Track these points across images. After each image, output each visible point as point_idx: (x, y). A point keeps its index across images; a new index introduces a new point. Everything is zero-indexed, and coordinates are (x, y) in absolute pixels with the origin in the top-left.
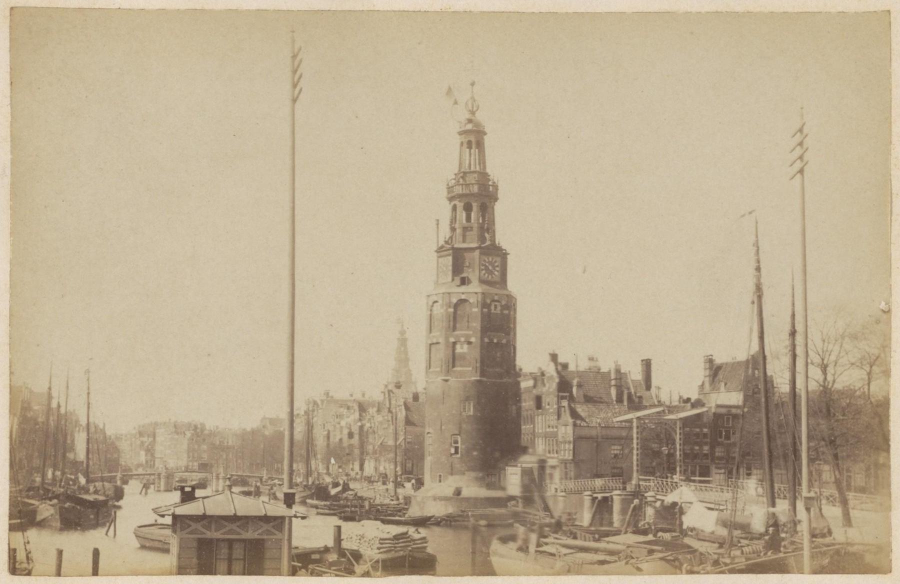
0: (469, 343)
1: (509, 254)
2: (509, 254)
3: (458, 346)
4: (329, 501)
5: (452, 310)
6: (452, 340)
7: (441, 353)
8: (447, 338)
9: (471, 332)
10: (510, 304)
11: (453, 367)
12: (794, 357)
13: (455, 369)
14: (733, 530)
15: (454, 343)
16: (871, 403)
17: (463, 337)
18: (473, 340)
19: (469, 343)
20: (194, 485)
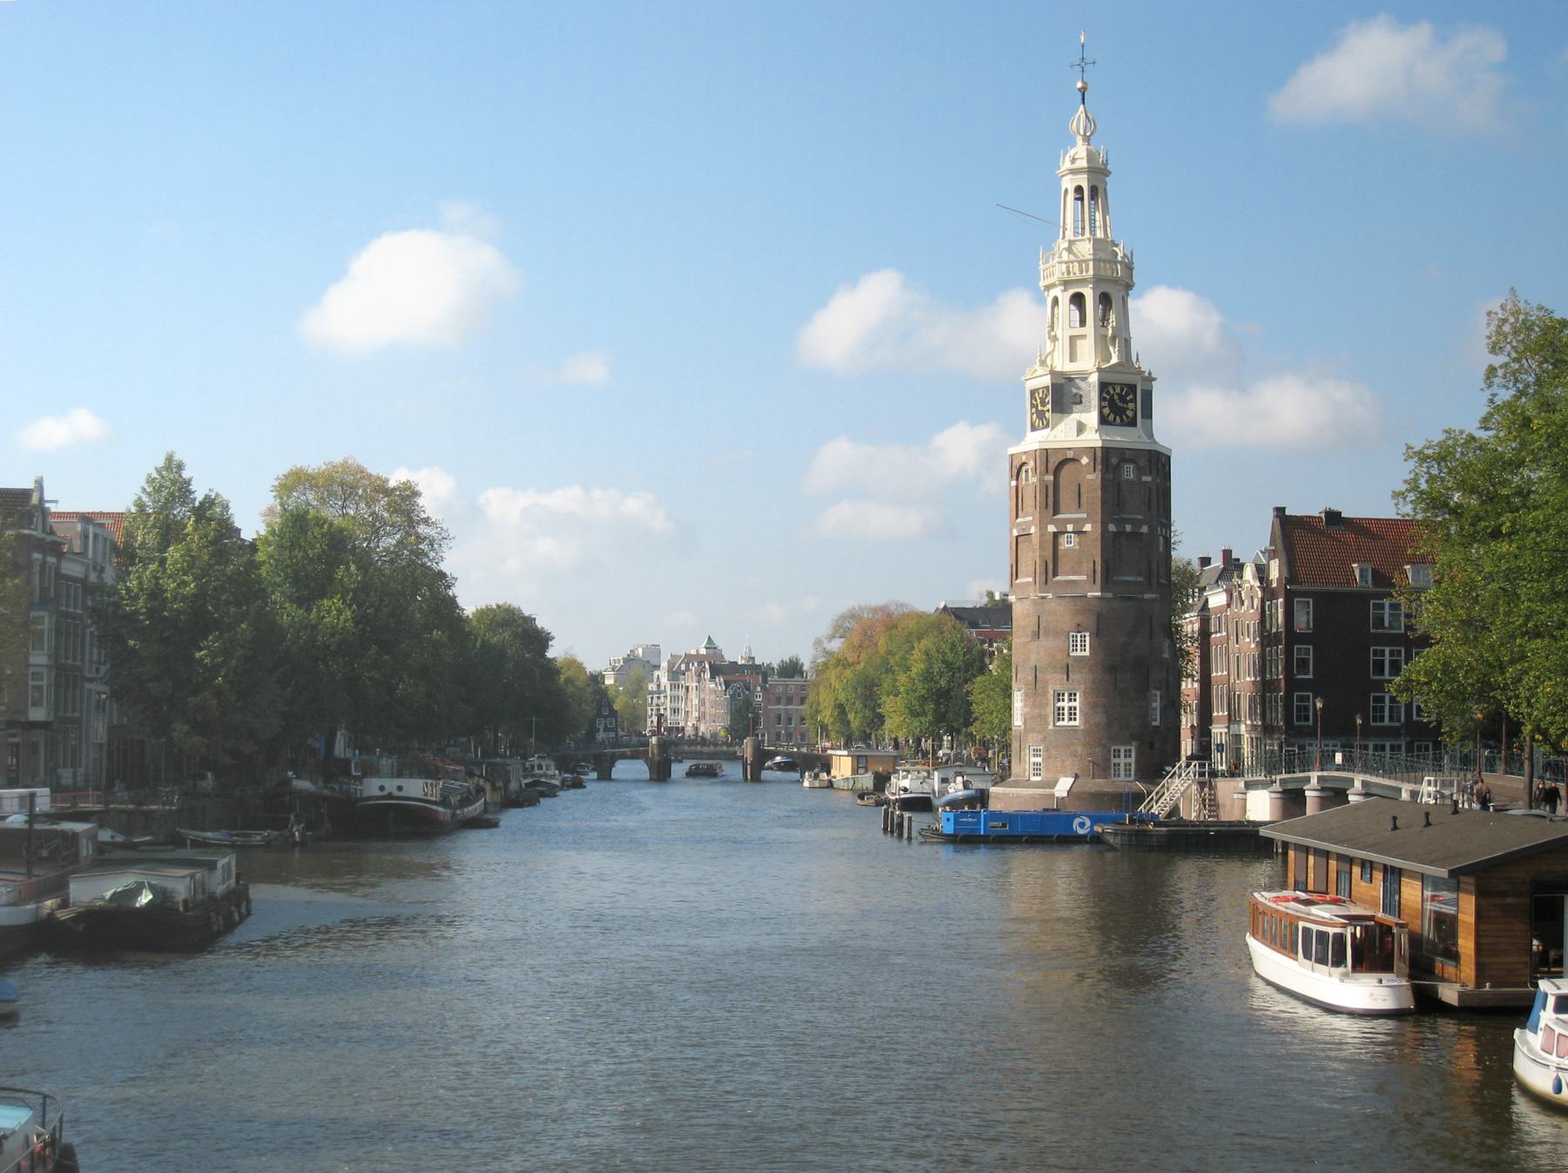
0: (1079, 533)
1: (1155, 379)
2: (1155, 379)
3: (1063, 539)
4: (427, 772)
5: (1051, 478)
6: (1052, 528)
7: (1032, 556)
8: (1043, 528)
9: (1085, 516)
10: (1158, 463)
11: (1055, 574)
12: (1047, 497)
13: (1058, 578)
14: (51, 719)
15: (1056, 535)
16: (167, 516)
17: (1107, 527)
18: (1088, 527)
19: (1079, 533)
20: (1446, 914)
